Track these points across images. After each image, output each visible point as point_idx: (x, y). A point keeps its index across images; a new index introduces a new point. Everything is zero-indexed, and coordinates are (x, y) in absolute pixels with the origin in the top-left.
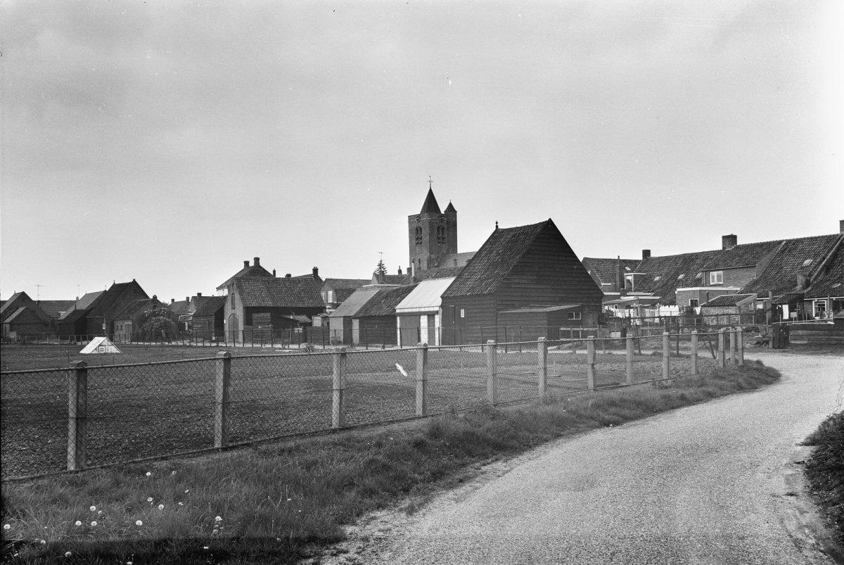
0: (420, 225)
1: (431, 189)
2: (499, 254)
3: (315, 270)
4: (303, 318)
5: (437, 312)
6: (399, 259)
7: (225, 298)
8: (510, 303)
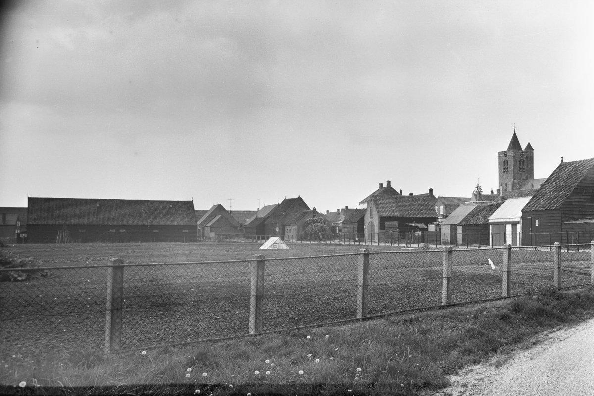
0: (507, 158)
1: (515, 134)
2: (563, 180)
3: (431, 191)
4: (421, 225)
5: (519, 222)
6: (491, 184)
7: (365, 210)
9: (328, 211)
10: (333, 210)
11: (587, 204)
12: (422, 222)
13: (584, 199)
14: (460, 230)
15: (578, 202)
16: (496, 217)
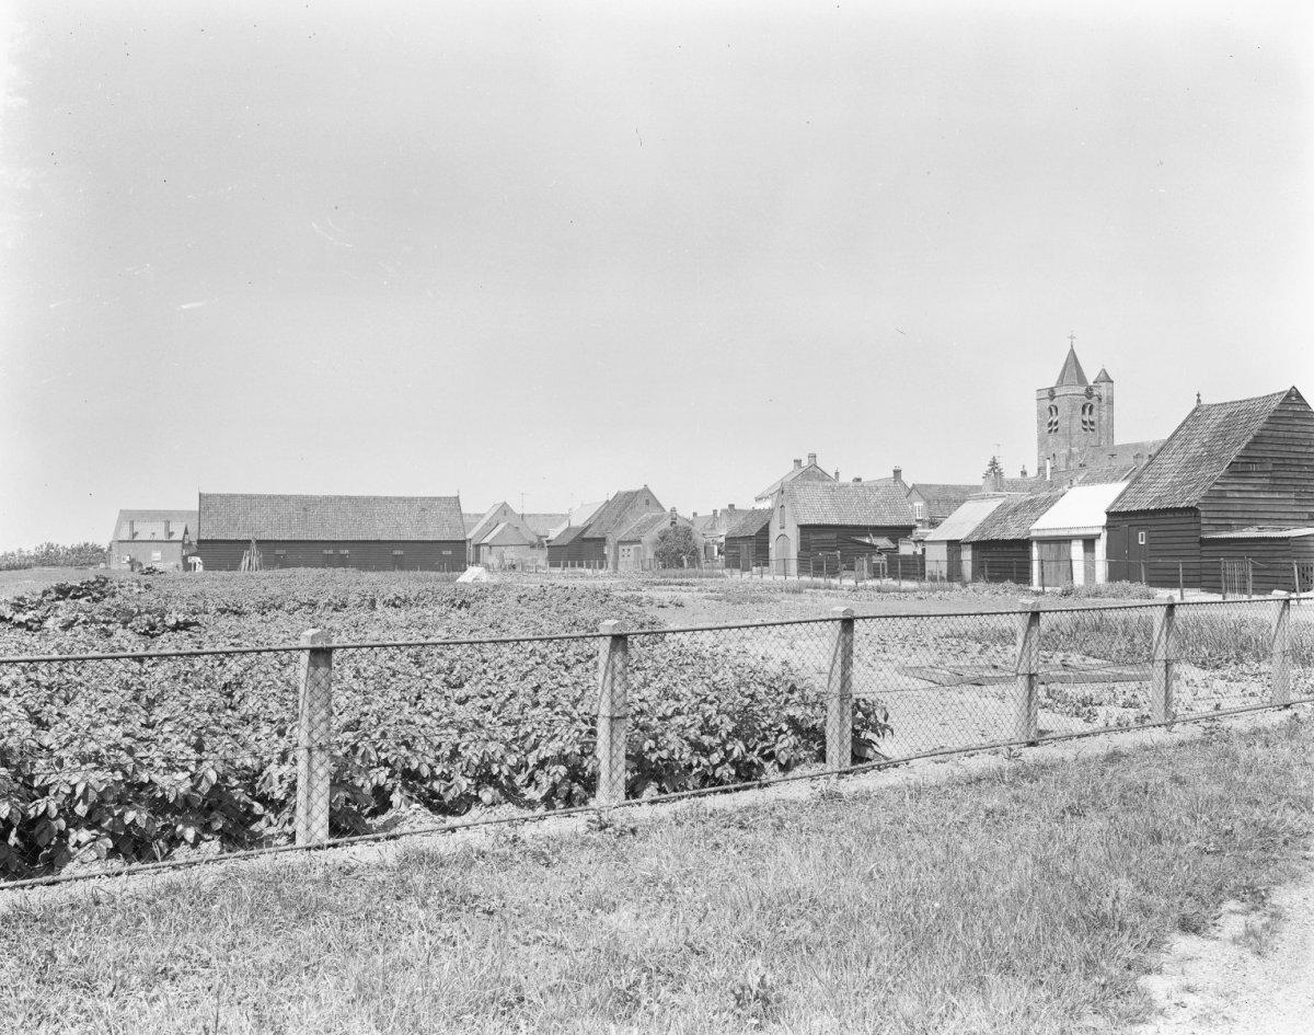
1: (1072, 351)
2: (1204, 445)
3: (897, 473)
4: (883, 542)
5: (1099, 536)
6: (1023, 457)
7: (771, 511)
8: (1223, 522)
9: (695, 514)
10: (705, 511)
11: (1262, 496)
12: (883, 536)
13: (1255, 485)
14: (967, 555)
15: (1239, 491)
16: (1050, 522)
